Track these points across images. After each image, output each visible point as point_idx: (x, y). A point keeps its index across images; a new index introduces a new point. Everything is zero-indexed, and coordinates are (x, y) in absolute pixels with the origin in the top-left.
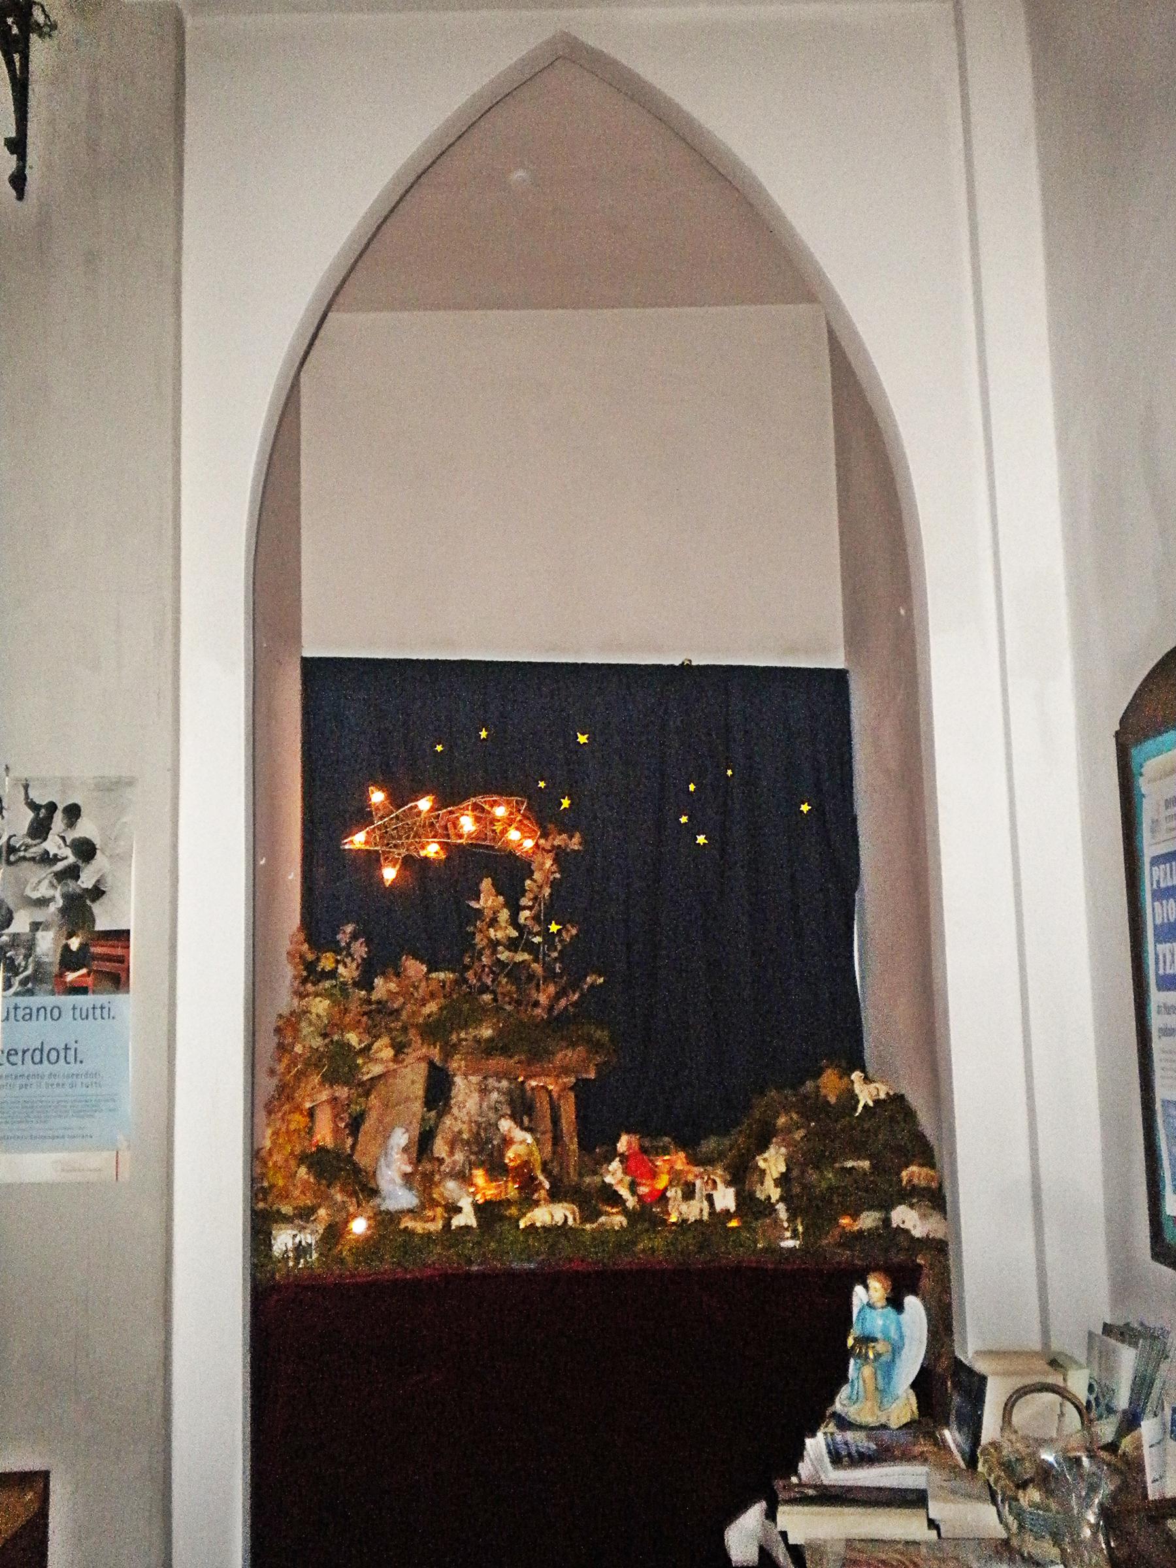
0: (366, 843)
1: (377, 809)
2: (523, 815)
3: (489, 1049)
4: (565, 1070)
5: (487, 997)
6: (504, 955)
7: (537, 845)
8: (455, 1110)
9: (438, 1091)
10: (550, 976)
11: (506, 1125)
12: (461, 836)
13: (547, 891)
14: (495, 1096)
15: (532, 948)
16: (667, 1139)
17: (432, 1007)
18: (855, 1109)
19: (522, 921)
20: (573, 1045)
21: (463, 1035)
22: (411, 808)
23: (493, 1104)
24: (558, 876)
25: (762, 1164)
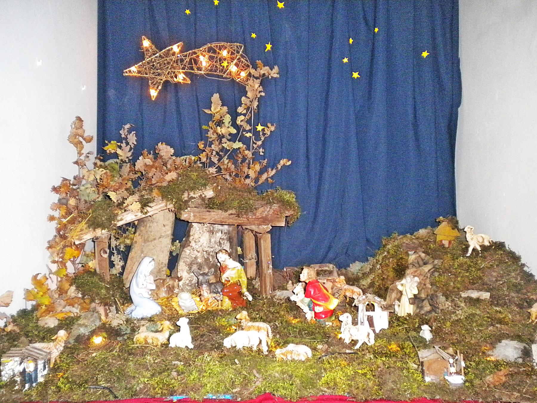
0: (139, 72)
1: (147, 50)
2: (241, 55)
3: (210, 204)
4: (265, 220)
5: (213, 170)
6: (227, 145)
7: (250, 75)
8: (193, 244)
9: (181, 231)
10: (256, 157)
11: (223, 257)
12: (199, 69)
13: (256, 104)
14: (219, 235)
15: (246, 141)
16: (331, 266)
17: (172, 176)
18: (467, 251)
19: (238, 122)
20: (270, 203)
21: (192, 194)
22: (169, 50)
23: (218, 240)
24: (263, 94)
25: (400, 288)
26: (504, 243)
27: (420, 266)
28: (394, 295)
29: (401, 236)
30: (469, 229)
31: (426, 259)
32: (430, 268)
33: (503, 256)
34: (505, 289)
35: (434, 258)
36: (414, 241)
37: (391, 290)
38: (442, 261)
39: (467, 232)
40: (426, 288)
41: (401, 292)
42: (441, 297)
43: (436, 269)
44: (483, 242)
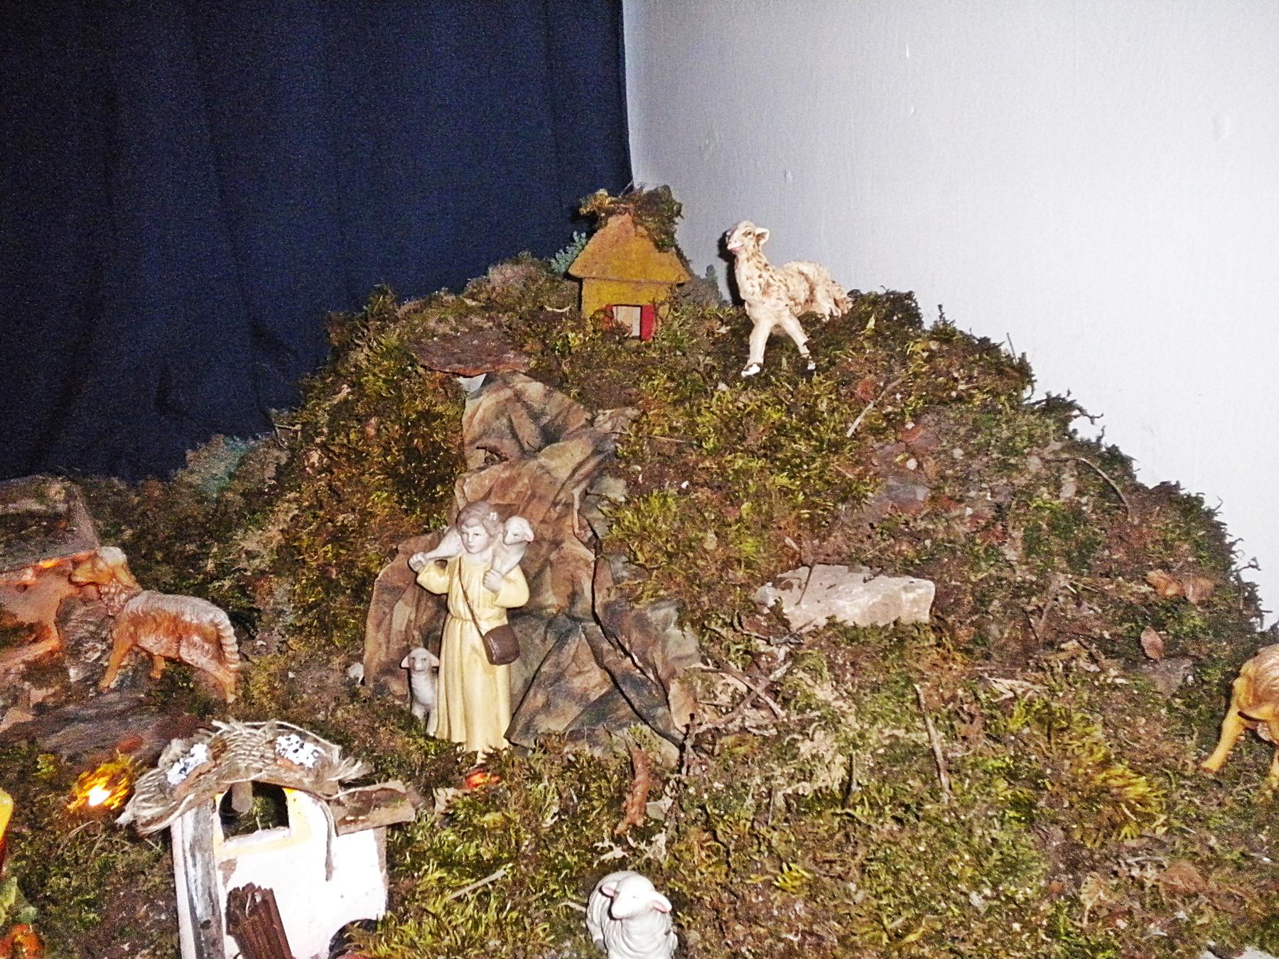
16: (56, 489)
18: (743, 358)
25: (433, 579)
26: (909, 295)
27: (527, 454)
28: (403, 614)
29: (408, 305)
30: (750, 242)
31: (552, 409)
32: (579, 458)
33: (941, 363)
34: (1011, 555)
35: (592, 400)
36: (476, 320)
37: (385, 589)
38: (631, 412)
39: (742, 257)
40: (563, 559)
41: (441, 603)
42: (673, 631)
43: (608, 462)
44: (811, 300)
